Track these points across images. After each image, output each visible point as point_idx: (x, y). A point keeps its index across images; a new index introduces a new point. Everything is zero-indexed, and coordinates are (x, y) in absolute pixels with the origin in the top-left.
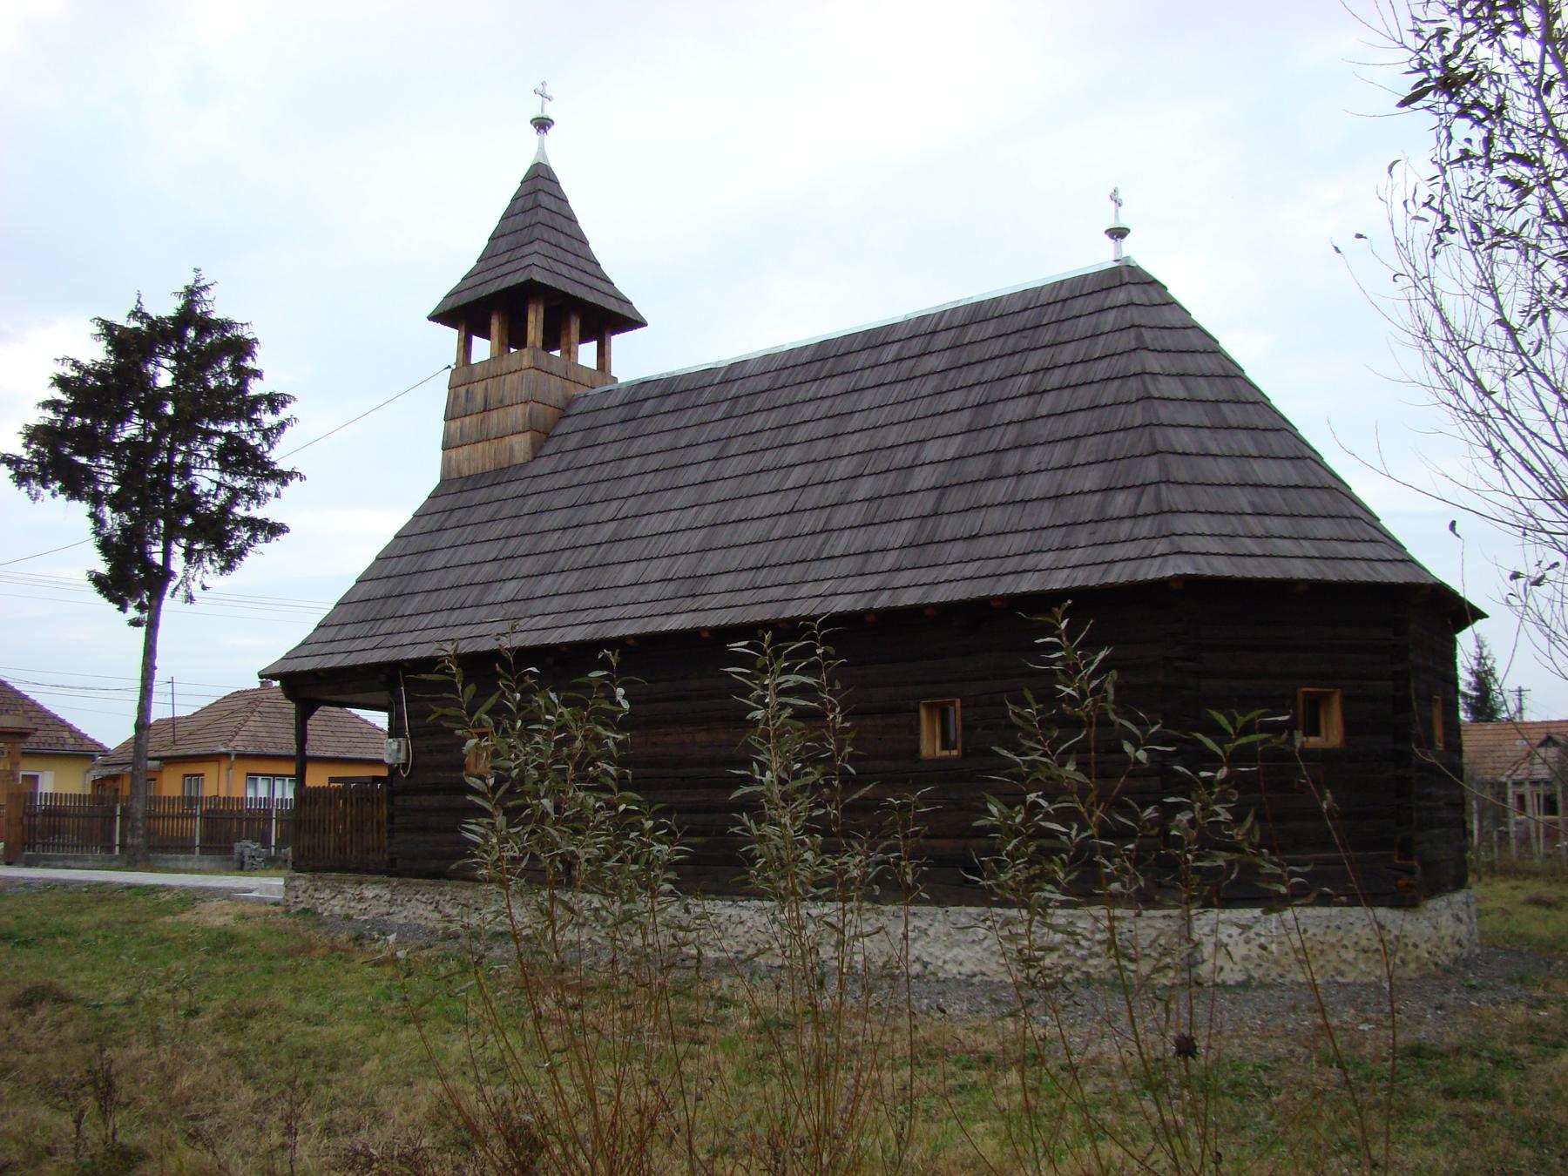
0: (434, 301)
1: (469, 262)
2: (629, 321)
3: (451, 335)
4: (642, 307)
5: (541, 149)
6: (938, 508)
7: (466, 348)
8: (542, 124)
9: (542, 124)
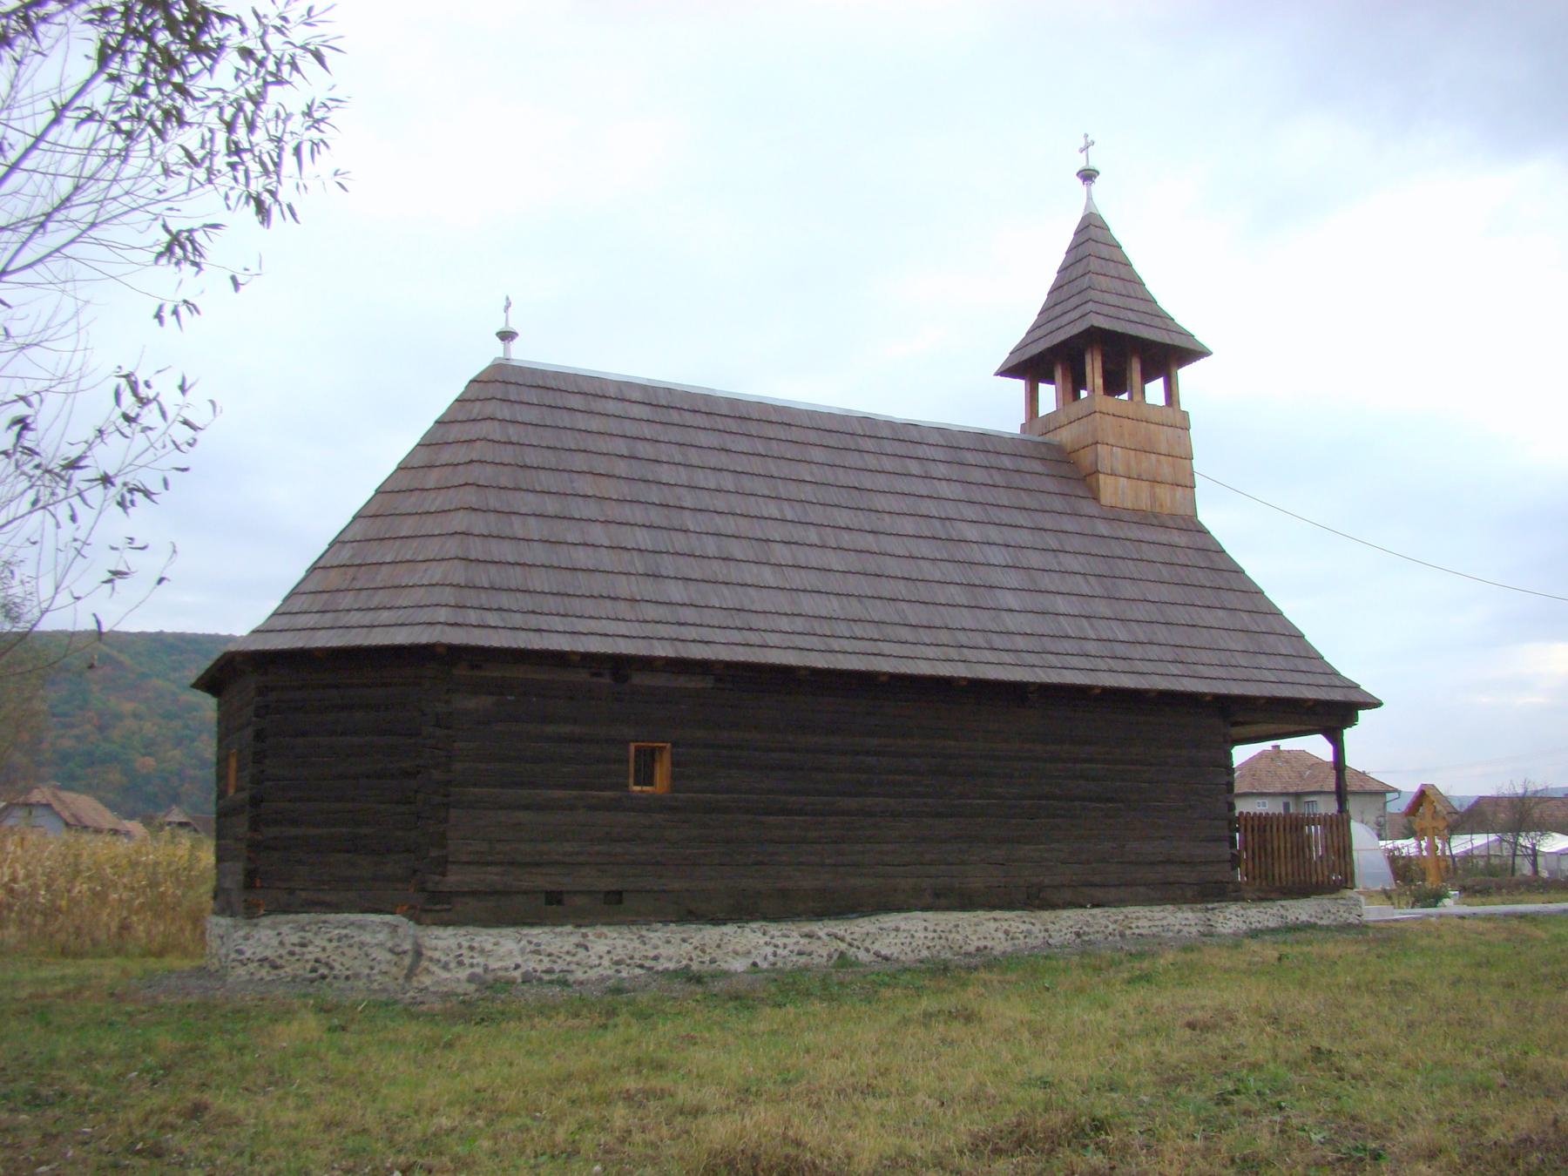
0: (1001, 357)
1: (1030, 317)
2: (1188, 352)
3: (1019, 386)
4: (1203, 337)
5: (1089, 198)
6: (87, 538)
7: (1032, 398)
8: (1088, 176)
9: (1088, 176)
